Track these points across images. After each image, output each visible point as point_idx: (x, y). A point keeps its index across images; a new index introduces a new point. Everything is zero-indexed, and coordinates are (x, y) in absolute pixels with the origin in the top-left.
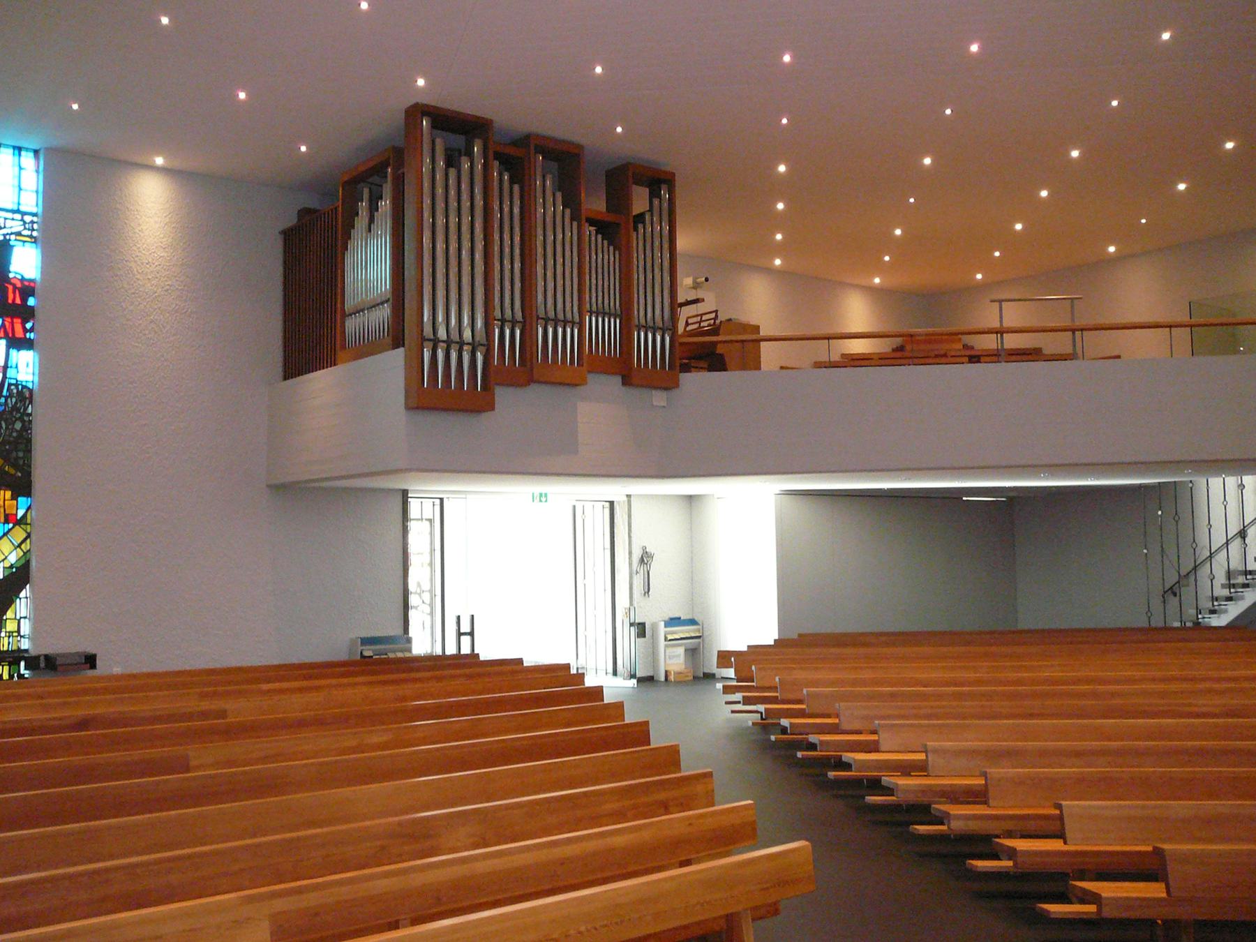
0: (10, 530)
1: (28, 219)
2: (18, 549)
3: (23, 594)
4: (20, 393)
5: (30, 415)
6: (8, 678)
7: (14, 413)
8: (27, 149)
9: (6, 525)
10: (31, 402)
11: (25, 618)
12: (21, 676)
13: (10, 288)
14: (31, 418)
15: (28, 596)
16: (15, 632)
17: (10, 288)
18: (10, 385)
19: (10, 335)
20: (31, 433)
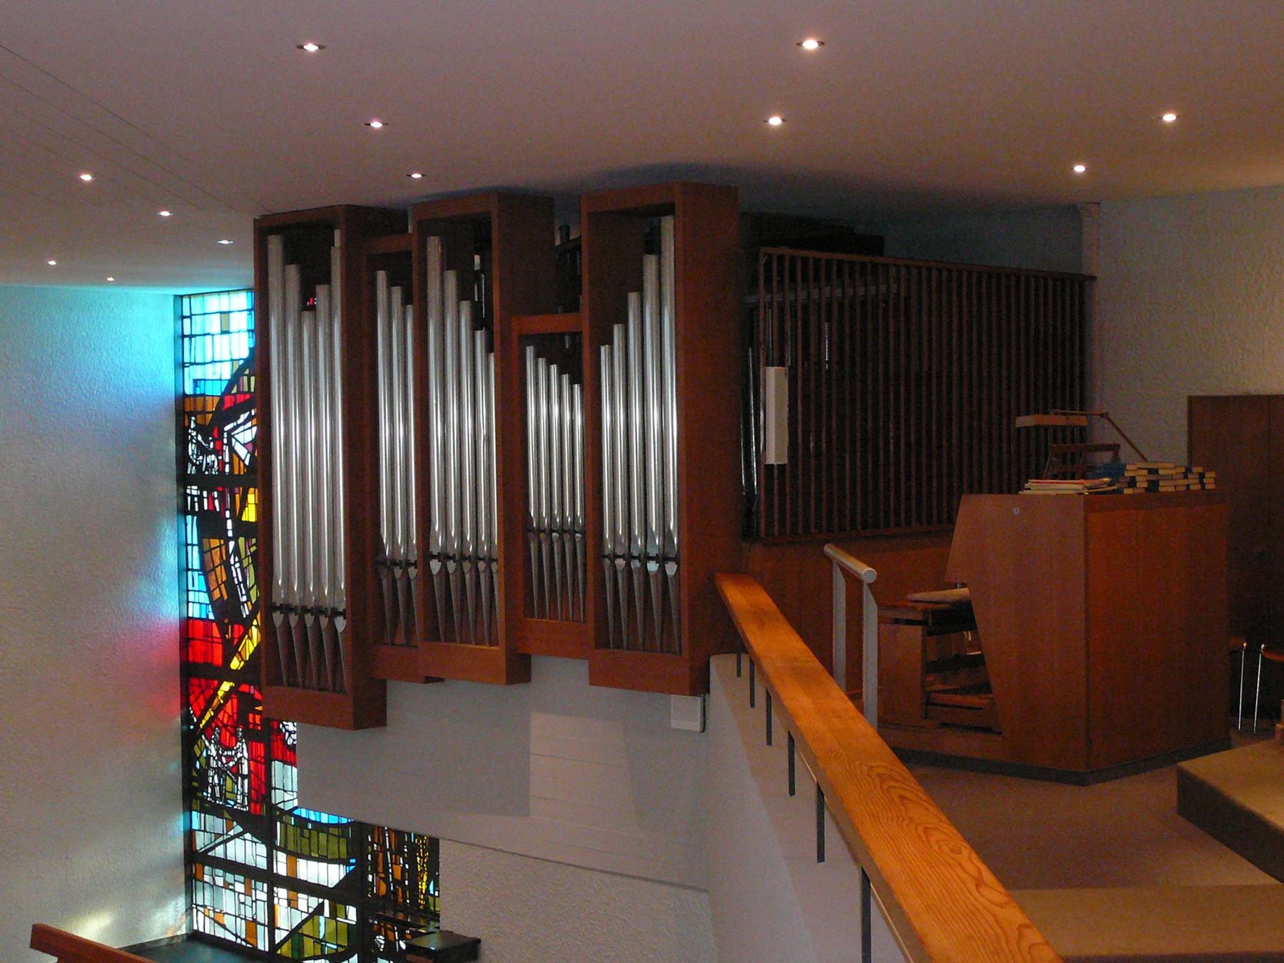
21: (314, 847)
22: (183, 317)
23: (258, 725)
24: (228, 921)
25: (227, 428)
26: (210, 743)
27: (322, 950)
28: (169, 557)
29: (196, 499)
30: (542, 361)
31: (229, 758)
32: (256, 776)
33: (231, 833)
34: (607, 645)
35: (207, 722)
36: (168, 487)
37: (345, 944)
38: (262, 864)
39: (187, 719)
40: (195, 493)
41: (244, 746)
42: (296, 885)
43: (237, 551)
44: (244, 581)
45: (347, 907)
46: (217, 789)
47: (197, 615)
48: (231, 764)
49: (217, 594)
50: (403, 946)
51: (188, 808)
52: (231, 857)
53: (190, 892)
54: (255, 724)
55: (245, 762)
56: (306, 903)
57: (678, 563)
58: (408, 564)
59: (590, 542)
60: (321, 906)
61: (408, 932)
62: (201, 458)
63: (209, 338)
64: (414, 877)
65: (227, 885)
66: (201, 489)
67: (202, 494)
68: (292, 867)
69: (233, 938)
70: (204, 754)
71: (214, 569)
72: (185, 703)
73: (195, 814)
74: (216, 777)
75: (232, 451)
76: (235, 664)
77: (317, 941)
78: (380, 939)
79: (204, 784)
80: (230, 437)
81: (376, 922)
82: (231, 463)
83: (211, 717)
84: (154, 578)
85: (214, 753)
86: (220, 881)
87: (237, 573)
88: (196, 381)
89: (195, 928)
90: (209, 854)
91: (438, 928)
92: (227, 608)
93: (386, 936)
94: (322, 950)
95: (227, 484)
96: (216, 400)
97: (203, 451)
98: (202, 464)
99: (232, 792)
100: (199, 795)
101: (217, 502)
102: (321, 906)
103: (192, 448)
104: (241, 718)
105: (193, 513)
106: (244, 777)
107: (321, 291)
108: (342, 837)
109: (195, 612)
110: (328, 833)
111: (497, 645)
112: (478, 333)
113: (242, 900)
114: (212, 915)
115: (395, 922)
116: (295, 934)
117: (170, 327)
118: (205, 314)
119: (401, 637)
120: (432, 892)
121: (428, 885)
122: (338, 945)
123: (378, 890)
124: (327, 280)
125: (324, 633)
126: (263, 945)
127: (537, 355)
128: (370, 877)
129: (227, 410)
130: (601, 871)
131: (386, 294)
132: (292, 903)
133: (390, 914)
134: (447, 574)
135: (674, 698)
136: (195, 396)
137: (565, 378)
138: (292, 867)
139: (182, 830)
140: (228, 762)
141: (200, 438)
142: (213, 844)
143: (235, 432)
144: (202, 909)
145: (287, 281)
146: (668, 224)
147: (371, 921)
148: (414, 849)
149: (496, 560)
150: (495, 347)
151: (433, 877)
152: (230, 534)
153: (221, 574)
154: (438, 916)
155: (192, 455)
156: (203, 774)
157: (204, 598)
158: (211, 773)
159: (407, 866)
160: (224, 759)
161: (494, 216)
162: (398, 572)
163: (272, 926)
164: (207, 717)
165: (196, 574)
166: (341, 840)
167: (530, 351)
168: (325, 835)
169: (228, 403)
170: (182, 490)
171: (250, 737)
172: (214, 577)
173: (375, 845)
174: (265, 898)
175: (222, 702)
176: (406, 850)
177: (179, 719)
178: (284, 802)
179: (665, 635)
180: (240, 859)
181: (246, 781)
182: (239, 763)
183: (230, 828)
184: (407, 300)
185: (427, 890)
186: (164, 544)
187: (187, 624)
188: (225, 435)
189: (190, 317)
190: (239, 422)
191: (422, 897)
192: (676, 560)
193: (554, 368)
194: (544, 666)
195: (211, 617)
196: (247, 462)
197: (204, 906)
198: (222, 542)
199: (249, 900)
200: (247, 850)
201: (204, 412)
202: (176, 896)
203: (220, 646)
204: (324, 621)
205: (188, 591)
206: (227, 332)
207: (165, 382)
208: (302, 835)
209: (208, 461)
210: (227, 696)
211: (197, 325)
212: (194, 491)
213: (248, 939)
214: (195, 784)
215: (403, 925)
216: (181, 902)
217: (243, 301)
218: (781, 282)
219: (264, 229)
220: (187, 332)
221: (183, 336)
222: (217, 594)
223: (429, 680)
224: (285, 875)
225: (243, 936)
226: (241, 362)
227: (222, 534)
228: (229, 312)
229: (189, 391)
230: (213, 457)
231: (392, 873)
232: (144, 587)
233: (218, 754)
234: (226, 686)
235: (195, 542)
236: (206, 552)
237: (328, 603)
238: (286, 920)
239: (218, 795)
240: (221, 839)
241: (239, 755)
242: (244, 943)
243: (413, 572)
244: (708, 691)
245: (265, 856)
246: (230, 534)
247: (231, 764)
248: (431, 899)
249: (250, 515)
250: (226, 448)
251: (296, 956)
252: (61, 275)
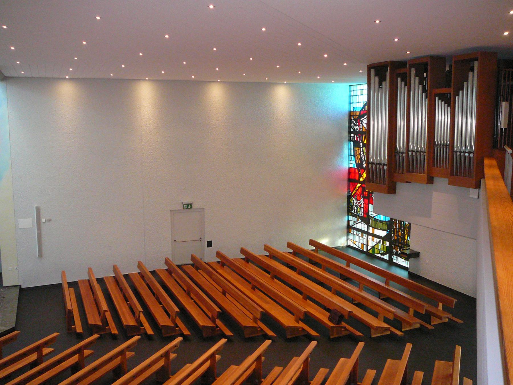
21: (379, 226)
22: (351, 91)
23: (366, 195)
24: (357, 243)
25: (361, 119)
26: (354, 199)
27: (380, 252)
28: (346, 152)
29: (353, 137)
30: (440, 101)
31: (359, 203)
32: (366, 207)
33: (359, 222)
34: (453, 175)
35: (354, 194)
36: (346, 134)
37: (386, 251)
38: (366, 230)
39: (349, 193)
40: (353, 136)
41: (363, 200)
42: (374, 236)
43: (363, 151)
44: (364, 159)
46: (356, 210)
47: (352, 167)
48: (359, 204)
49: (357, 162)
50: (400, 252)
51: (348, 215)
52: (358, 228)
53: (348, 235)
54: (366, 195)
55: (363, 204)
56: (376, 240)
57: (473, 154)
58: (403, 153)
59: (451, 148)
60: (380, 241)
61: (402, 249)
62: (354, 127)
63: (357, 96)
64: (404, 235)
65: (357, 234)
66: (354, 135)
67: (354, 136)
68: (373, 231)
69: (358, 248)
70: (353, 202)
71: (357, 155)
72: (349, 189)
73: (350, 216)
74: (355, 207)
75: (362, 125)
76: (361, 179)
77: (379, 250)
78: (394, 250)
79: (352, 209)
80: (362, 122)
81: (394, 246)
82: (362, 128)
83: (355, 193)
84: (342, 157)
85: (355, 201)
86: (355, 233)
87: (362, 156)
88: (354, 107)
89: (349, 244)
90: (353, 226)
91: (409, 249)
92: (359, 165)
93: (396, 250)
94: (380, 252)
95: (359, 133)
96: (359, 112)
97: (355, 125)
98: (355, 129)
99: (359, 211)
100: (351, 212)
101: (358, 138)
102: (380, 241)
103: (352, 124)
104: (362, 193)
105: (352, 141)
106: (362, 208)
107: (384, 83)
108: (386, 224)
109: (352, 166)
110: (383, 223)
111: (425, 174)
112: (424, 93)
113: (360, 238)
114: (353, 241)
115: (398, 246)
116: (373, 248)
117: (347, 93)
118: (356, 90)
119: (401, 172)
120: (408, 240)
121: (407, 238)
122: (384, 251)
123: (395, 238)
124: (385, 80)
125: (381, 170)
126: (365, 250)
127: (439, 99)
128: (393, 235)
129: (361, 116)
131: (400, 84)
132: (372, 240)
133: (397, 244)
134: (413, 156)
135: (471, 189)
136: (354, 111)
137: (446, 105)
138: (373, 231)
139: (346, 220)
140: (358, 204)
141: (354, 122)
143: (364, 120)
144: (350, 240)
145: (375, 80)
146: (476, 64)
147: (392, 246)
148: (404, 228)
149: (426, 152)
150: (428, 97)
151: (409, 236)
152: (361, 146)
153: (359, 156)
154: (410, 245)
156: (352, 206)
157: (354, 162)
158: (354, 206)
159: (402, 233)
160: (357, 203)
161: (429, 63)
162: (401, 155)
163: (367, 245)
164: (354, 192)
165: (353, 156)
166: (386, 225)
167: (437, 98)
168: (382, 223)
169: (362, 113)
170: (350, 135)
171: (364, 198)
172: (357, 157)
173: (394, 227)
174: (366, 238)
175: (358, 189)
176: (402, 228)
177: (347, 193)
179: (469, 174)
180: (360, 228)
181: (363, 209)
182: (361, 204)
183: (358, 220)
184: (406, 85)
185: (407, 239)
186: (345, 148)
187: (350, 169)
188: (361, 121)
189: (353, 91)
190: (365, 118)
191: (406, 241)
192: (473, 153)
193: (443, 102)
194: (436, 180)
195: (356, 167)
196: (366, 128)
197: (351, 239)
198: (359, 148)
199: (362, 239)
200: (362, 226)
201: (356, 115)
202: (344, 236)
203: (358, 175)
204: (381, 167)
205: (350, 161)
206: (362, 95)
207: (345, 108)
208: (376, 223)
209: (357, 128)
210: (359, 187)
211: (355, 93)
212: (352, 135)
213: (362, 248)
214: (350, 209)
215: (400, 248)
216: (345, 237)
217: (366, 86)
218: (509, 78)
219: (370, 68)
220: (352, 95)
221: (351, 96)
222: (357, 162)
223: (407, 182)
224: (371, 233)
225: (360, 247)
226: (366, 103)
227: (359, 147)
228: (363, 90)
229: (352, 110)
230: (357, 127)
231: (398, 234)
232: (339, 159)
233: (356, 202)
234: (359, 185)
235: (353, 148)
236: (355, 151)
237: (383, 162)
238: (371, 244)
239: (356, 212)
240: (356, 223)
241: (361, 202)
242: (360, 249)
243: (404, 155)
244: (480, 188)
246: (361, 146)
247: (359, 204)
248: (408, 241)
249: (365, 142)
250: (361, 125)
251: (373, 253)
252: (321, 80)
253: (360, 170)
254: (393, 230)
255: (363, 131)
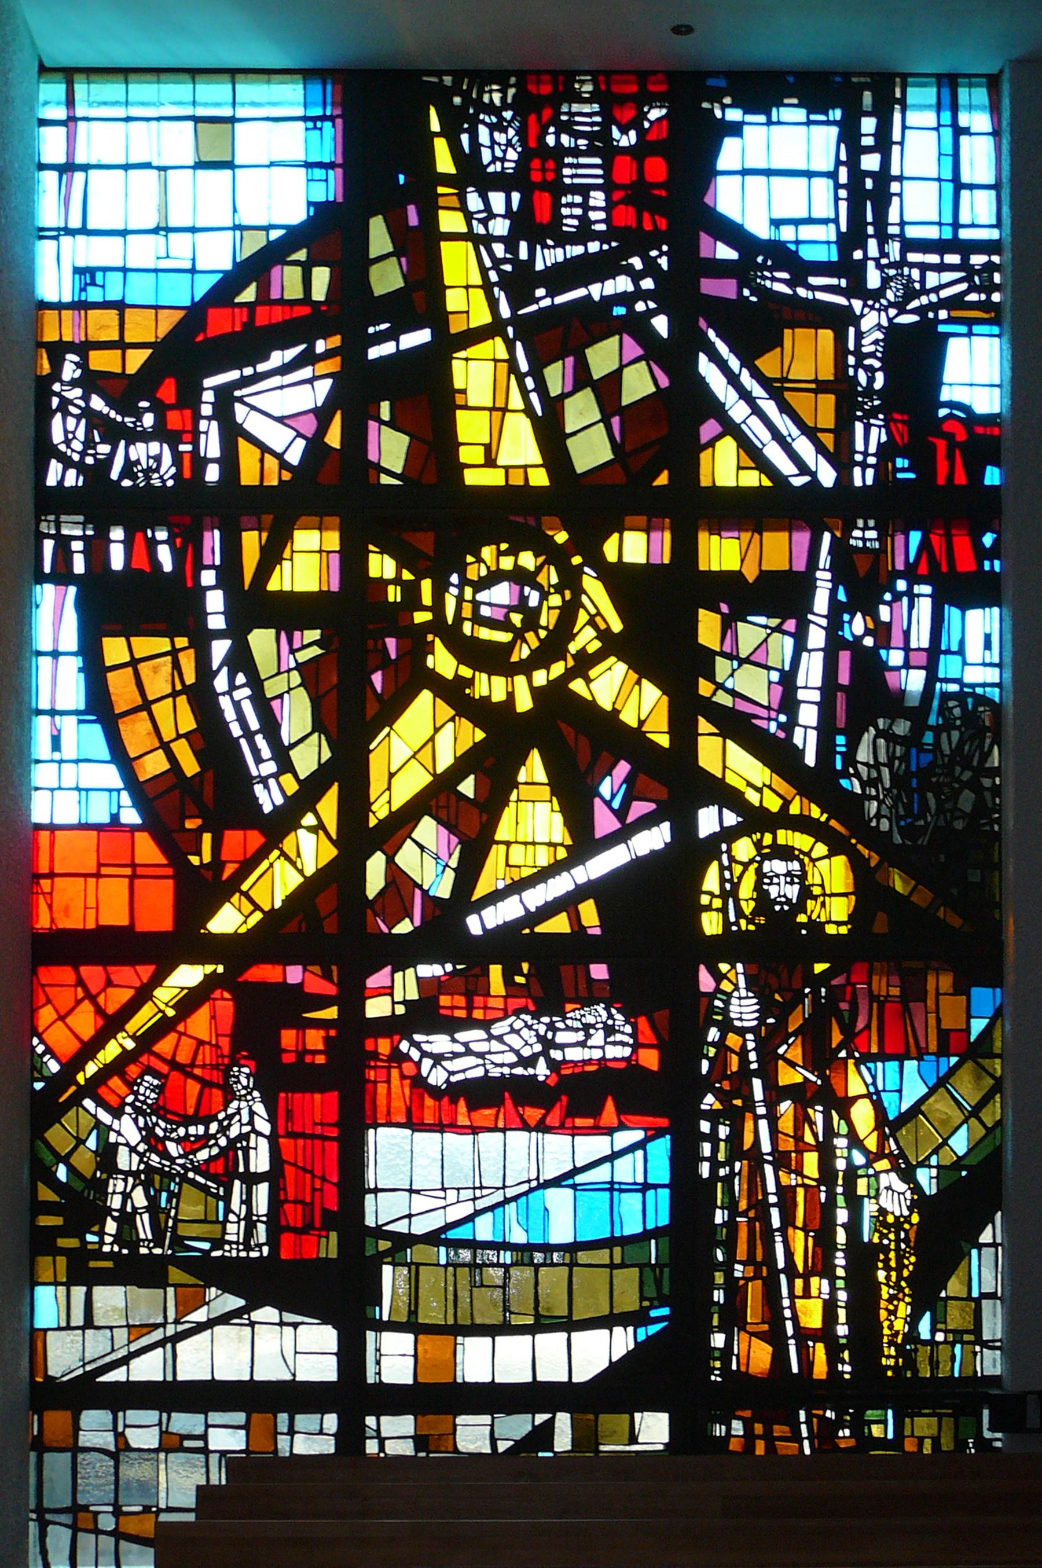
0: (952, 1071)
1: (978, 260)
2: (973, 1121)
3: (986, 1237)
4: (970, 718)
5: (996, 772)
6: (952, 1447)
7: (958, 769)
8: (971, 79)
9: (943, 1060)
10: (997, 741)
11: (992, 1296)
12: (984, 1444)
13: (941, 445)
14: (997, 781)
15: (999, 1240)
16: (968, 1332)
17: (941, 445)
18: (945, 696)
19: (944, 568)
20: (998, 821)
33: (200, 1315)
41: (259, 1108)
45: (637, 1416)
130: (167, 1488)
142: (123, 1353)
147: (614, 244)
152: (217, 622)
155: (67, 442)
175: (171, 1013)
178: (410, 1216)
182: (238, 1146)
195: (131, 816)
226: (275, 235)
245: (210, 1331)
246: (217, 622)
253: (207, 838)
254: (718, 1296)
255: (600, 181)
